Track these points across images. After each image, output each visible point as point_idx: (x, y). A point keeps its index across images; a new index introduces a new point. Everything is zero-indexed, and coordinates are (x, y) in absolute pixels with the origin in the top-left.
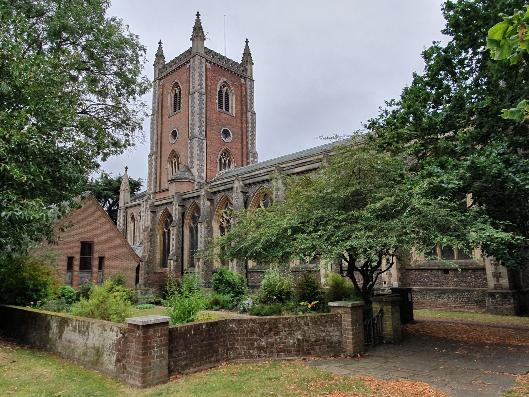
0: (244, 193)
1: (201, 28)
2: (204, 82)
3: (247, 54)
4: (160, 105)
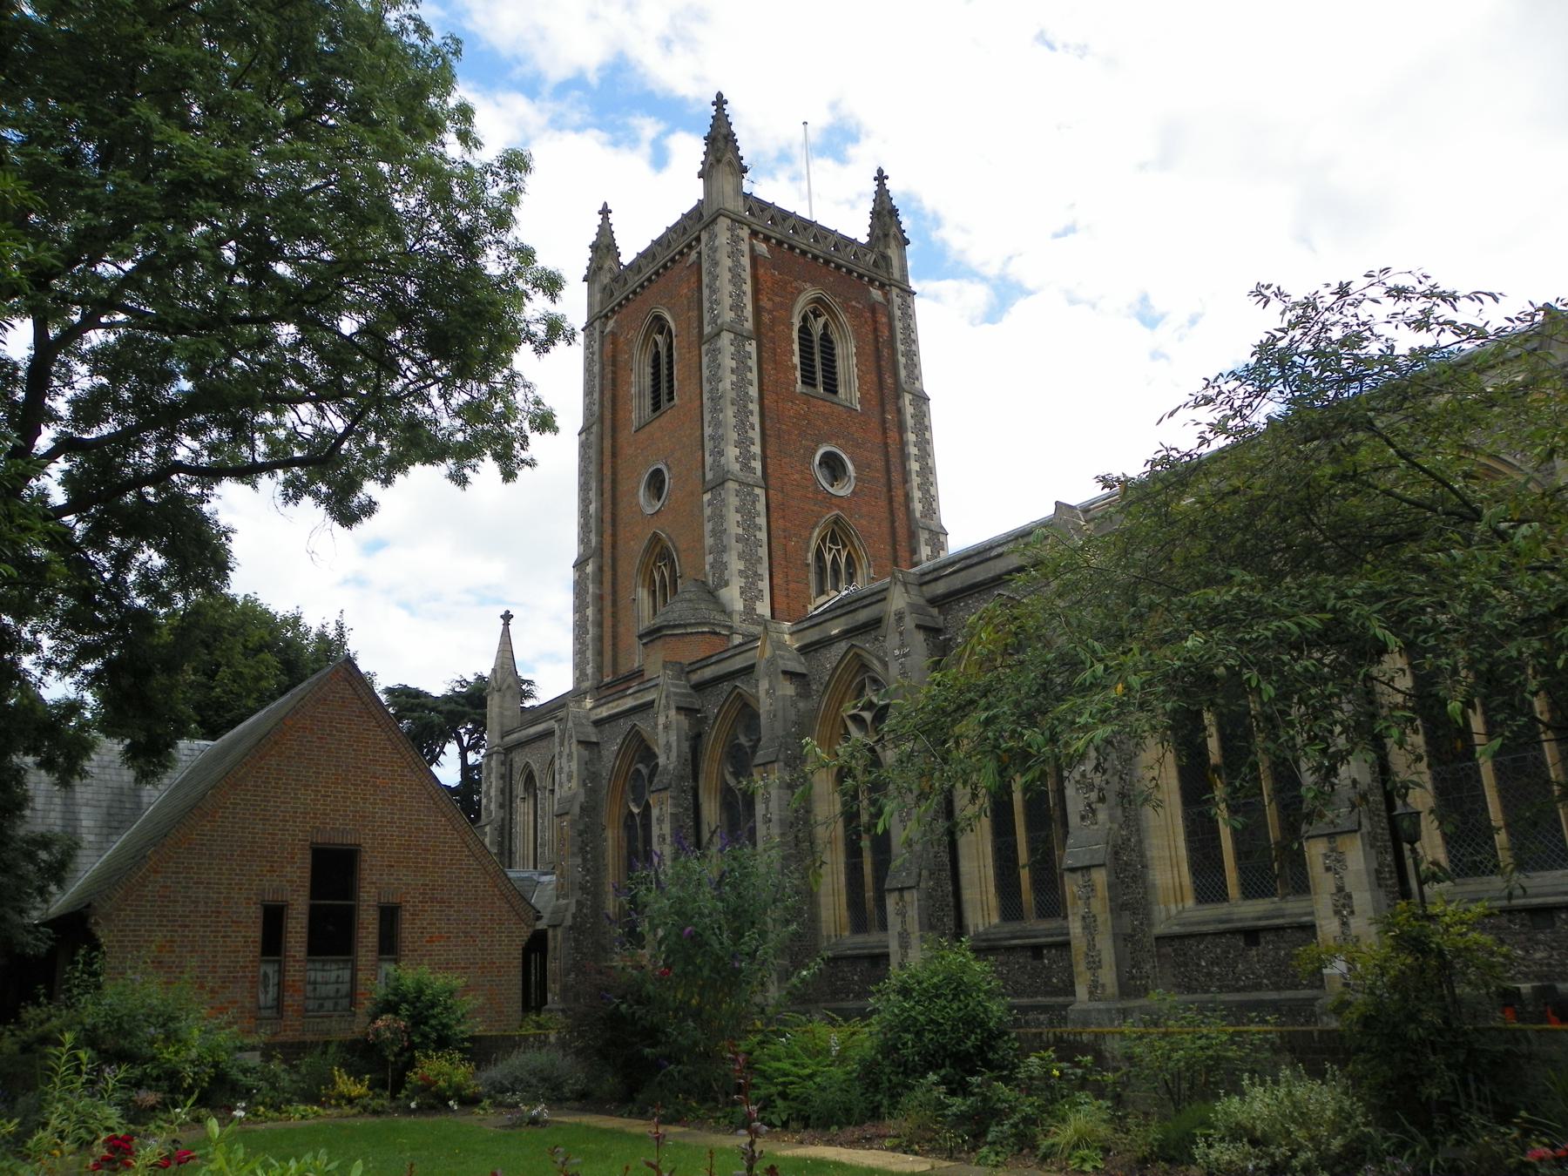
0: (931, 631)
1: (730, 139)
2: (748, 301)
3: (885, 213)
4: (608, 395)
